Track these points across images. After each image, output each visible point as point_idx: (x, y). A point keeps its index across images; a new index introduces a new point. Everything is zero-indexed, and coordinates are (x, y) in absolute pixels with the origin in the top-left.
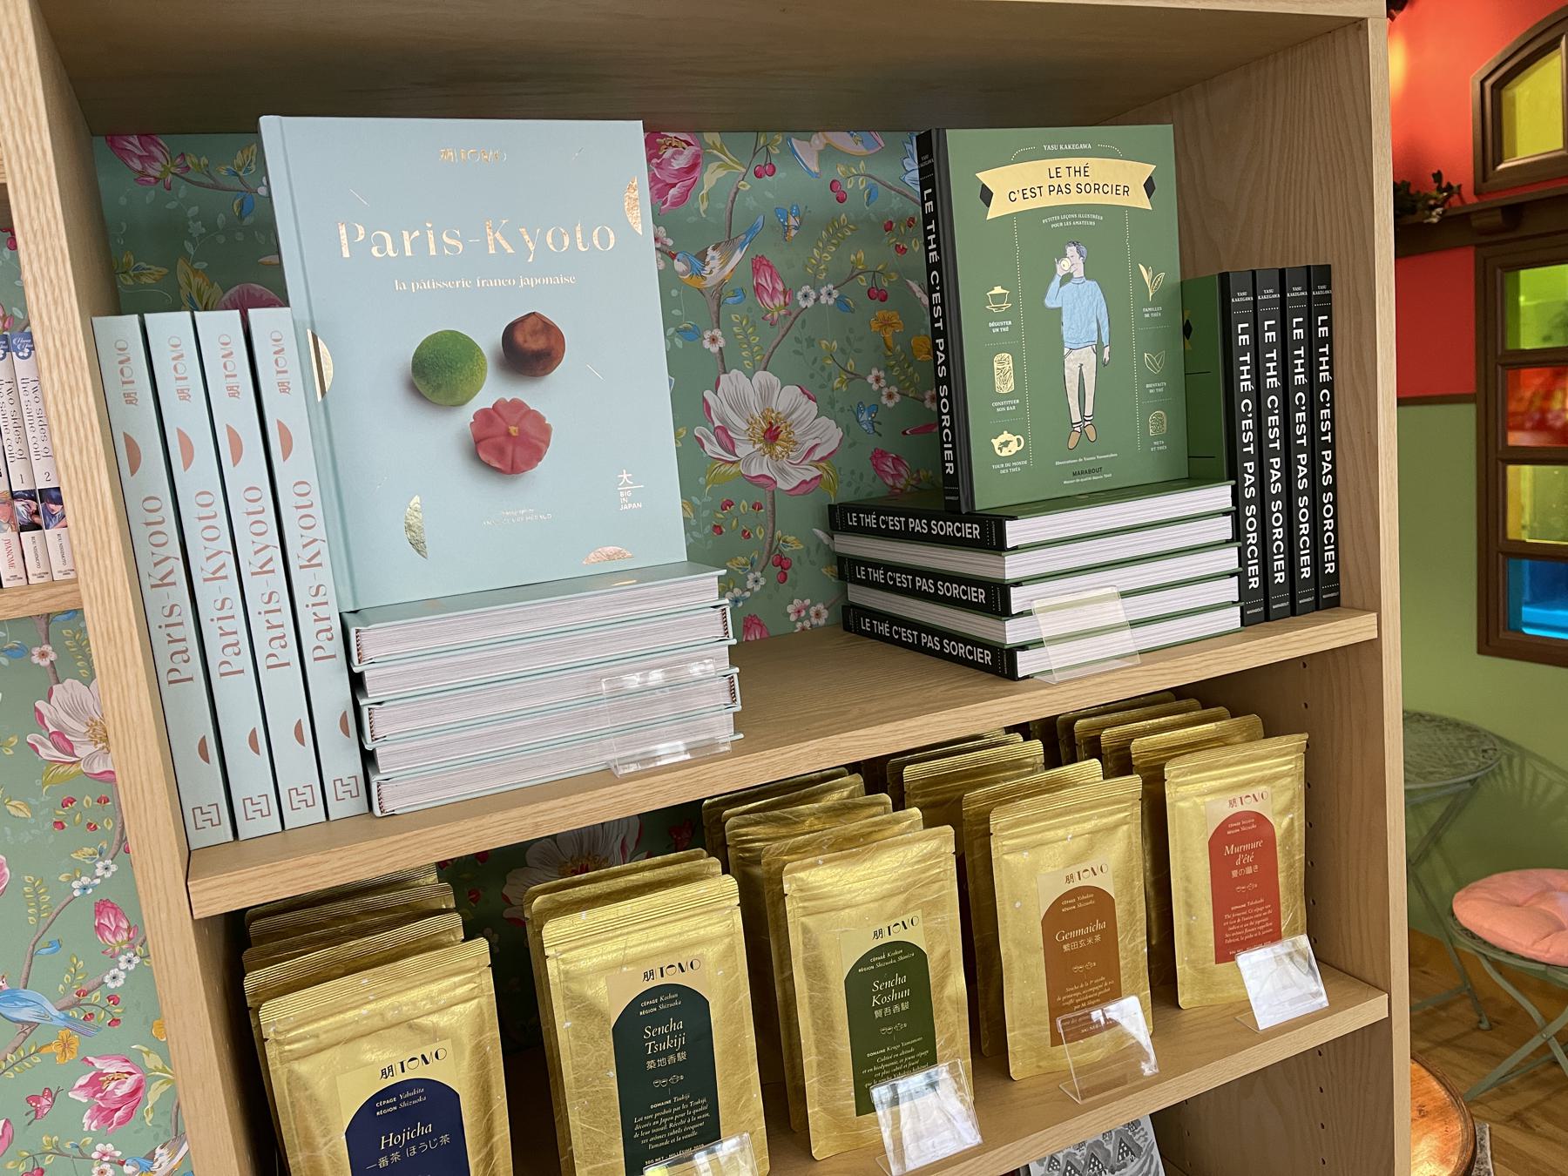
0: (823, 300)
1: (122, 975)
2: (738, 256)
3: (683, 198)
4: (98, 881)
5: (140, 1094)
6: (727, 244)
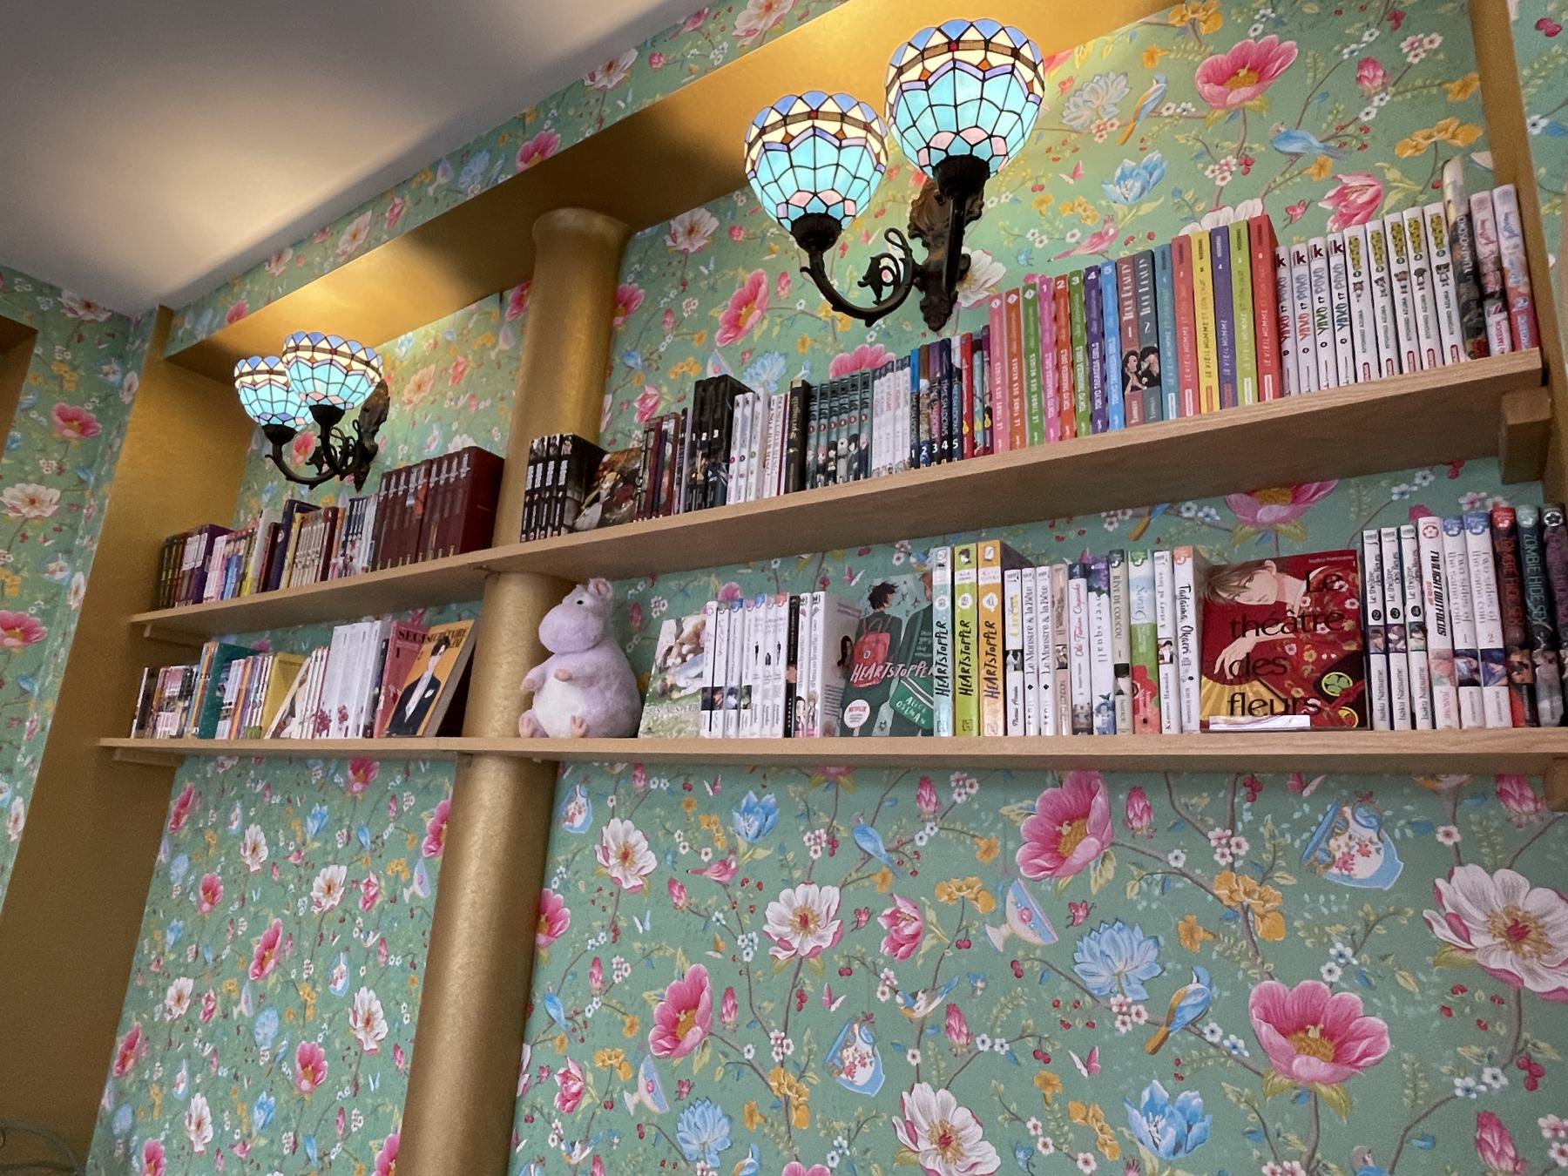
0: (997, 1048)
1: (1375, 111)
2: (938, 1001)
3: (907, 955)
4: (1415, 488)
5: (1378, 201)
6: (932, 992)
